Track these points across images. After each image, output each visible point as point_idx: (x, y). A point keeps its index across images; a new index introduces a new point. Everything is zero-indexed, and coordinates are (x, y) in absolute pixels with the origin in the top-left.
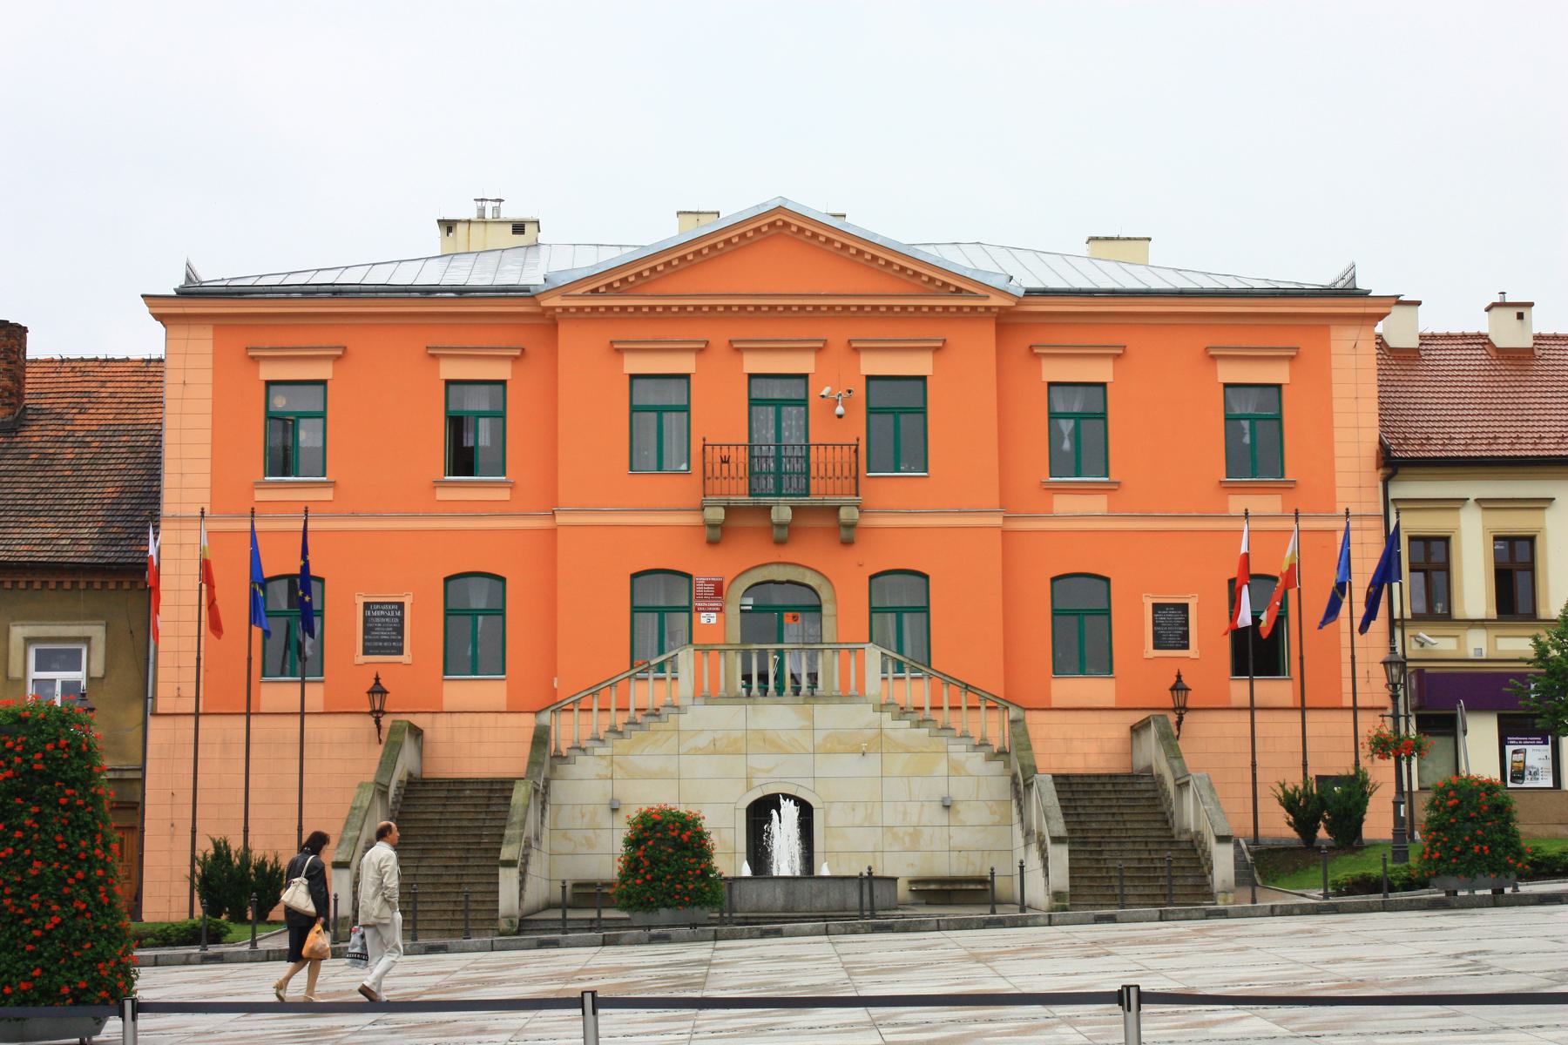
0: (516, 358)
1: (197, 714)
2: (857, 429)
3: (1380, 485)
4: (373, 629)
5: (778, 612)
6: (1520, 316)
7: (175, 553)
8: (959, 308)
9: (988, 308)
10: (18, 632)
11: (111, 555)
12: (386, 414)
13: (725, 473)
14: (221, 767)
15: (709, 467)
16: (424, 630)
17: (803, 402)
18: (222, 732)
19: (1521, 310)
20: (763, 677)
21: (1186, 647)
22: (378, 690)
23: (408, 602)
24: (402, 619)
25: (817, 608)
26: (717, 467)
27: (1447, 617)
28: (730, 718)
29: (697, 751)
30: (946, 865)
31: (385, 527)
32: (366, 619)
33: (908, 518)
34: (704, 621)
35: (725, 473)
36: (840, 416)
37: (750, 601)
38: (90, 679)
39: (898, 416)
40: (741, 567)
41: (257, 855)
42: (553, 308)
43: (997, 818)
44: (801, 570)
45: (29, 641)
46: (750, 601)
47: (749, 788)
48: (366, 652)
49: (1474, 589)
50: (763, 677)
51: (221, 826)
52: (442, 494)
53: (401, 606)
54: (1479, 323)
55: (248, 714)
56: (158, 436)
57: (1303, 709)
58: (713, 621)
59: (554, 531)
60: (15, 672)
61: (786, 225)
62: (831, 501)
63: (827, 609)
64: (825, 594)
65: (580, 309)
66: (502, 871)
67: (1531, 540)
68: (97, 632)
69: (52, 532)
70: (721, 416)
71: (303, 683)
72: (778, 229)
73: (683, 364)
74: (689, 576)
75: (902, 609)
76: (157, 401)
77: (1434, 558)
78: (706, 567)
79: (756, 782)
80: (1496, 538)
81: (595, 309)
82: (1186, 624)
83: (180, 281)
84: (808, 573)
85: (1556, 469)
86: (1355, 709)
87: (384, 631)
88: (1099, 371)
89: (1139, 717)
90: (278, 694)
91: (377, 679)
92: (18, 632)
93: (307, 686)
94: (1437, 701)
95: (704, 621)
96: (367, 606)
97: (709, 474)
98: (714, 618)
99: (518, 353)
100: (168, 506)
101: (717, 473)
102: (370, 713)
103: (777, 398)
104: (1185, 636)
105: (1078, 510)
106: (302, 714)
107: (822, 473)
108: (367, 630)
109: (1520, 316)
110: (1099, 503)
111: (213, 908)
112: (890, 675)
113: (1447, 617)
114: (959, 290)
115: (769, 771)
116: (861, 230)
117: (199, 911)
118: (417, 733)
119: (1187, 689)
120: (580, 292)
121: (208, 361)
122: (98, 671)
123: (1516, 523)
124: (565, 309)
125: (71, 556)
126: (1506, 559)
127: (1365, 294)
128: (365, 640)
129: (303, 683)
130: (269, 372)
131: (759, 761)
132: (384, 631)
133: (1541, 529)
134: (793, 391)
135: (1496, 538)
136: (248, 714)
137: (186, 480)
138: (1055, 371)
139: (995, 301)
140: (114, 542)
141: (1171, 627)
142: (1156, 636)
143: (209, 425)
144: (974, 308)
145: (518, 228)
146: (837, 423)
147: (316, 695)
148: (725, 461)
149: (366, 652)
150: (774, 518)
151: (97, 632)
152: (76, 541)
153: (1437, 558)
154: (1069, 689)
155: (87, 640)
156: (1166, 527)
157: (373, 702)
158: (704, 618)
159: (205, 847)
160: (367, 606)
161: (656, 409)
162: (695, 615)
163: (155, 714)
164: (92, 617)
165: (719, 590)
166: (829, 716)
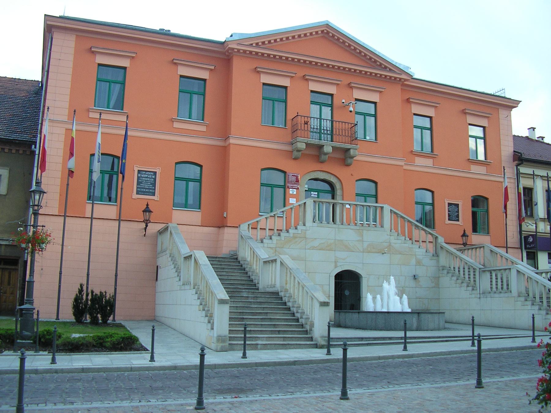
0: (211, 70)
3: (515, 167)
4: (141, 183)
8: (391, 77)
9: (400, 79)
13: (306, 129)
17: (331, 106)
21: (458, 220)
22: (147, 210)
23: (158, 171)
24: (155, 179)
26: (303, 125)
29: (313, 248)
31: (164, 135)
32: (138, 178)
34: (291, 192)
35: (306, 129)
36: (351, 111)
40: (305, 172)
42: (233, 49)
43: (433, 285)
44: (329, 175)
48: (137, 193)
52: (176, 125)
53: (155, 173)
57: (65, 216)
58: (295, 193)
61: (328, 33)
64: (338, 186)
65: (245, 51)
71: (93, 204)
72: (328, 34)
73: (285, 82)
74: (285, 172)
78: (290, 167)
79: (339, 264)
81: (251, 52)
82: (458, 212)
84: (332, 177)
85: (545, 166)
86: (92, 218)
91: (147, 205)
93: (95, 205)
95: (291, 192)
96: (139, 171)
98: (295, 192)
99: (213, 68)
101: (303, 128)
102: (143, 221)
104: (458, 216)
107: (338, 133)
108: (139, 183)
110: (429, 162)
114: (390, 70)
115: (344, 259)
116: (354, 37)
119: (468, 236)
120: (246, 44)
121: (72, 51)
124: (239, 50)
128: (137, 188)
129: (93, 204)
132: (147, 185)
137: (57, 106)
139: (403, 76)
142: (449, 215)
144: (395, 78)
149: (137, 193)
158: (292, 191)
160: (139, 171)
162: (287, 190)
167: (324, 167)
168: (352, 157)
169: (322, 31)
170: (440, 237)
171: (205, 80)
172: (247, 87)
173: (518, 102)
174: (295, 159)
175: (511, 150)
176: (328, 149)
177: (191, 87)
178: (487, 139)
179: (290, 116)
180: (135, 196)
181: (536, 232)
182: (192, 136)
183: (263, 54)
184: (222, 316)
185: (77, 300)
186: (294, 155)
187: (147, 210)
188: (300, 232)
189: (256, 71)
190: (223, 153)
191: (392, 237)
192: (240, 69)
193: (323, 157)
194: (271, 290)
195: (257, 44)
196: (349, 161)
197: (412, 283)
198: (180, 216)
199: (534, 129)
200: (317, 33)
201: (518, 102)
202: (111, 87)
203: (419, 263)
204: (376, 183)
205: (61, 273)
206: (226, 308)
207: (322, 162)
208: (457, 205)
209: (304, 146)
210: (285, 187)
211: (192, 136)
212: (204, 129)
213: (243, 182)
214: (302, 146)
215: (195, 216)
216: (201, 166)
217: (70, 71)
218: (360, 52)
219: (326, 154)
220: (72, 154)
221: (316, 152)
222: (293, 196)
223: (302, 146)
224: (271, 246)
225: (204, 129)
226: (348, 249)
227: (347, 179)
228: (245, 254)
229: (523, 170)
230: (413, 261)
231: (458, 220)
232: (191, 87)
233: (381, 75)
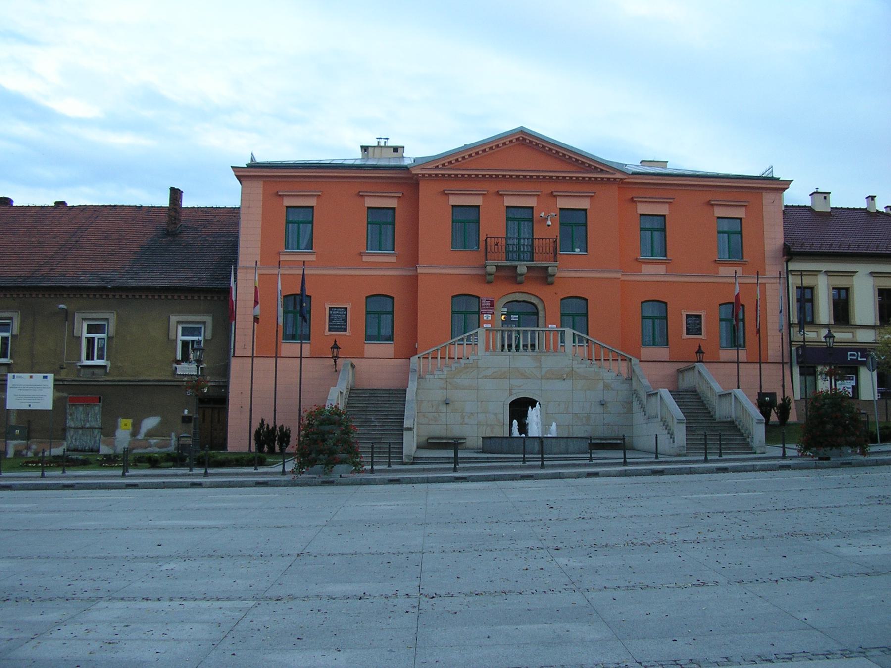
1: (253, 357)
2: (556, 232)
5: (529, 313)
6: (825, 198)
7: (244, 287)
9: (615, 179)
10: (174, 319)
11: (217, 285)
12: (341, 220)
14: (265, 384)
15: (489, 248)
16: (356, 320)
17: (531, 220)
18: (265, 365)
19: (826, 195)
20: (510, 346)
21: (701, 334)
22: (335, 347)
23: (349, 307)
24: (346, 315)
25: (537, 314)
27: (812, 323)
28: (503, 360)
29: (486, 377)
30: (601, 432)
32: (330, 315)
33: (574, 272)
37: (506, 310)
38: (206, 341)
39: (574, 224)
40: (503, 295)
41: (278, 425)
42: (417, 174)
45: (179, 322)
46: (506, 310)
47: (511, 395)
48: (329, 330)
49: (824, 312)
50: (510, 346)
51: (263, 413)
52: (365, 259)
53: (346, 309)
54: (808, 202)
55: (276, 357)
56: (237, 237)
59: (417, 276)
60: (172, 337)
61: (524, 139)
62: (545, 264)
63: (541, 314)
64: (540, 307)
65: (430, 175)
66: (405, 433)
67: (847, 290)
68: (208, 319)
69: (190, 275)
70: (493, 225)
71: (302, 344)
72: (523, 140)
74: (479, 298)
75: (576, 312)
76: (237, 224)
77: (807, 297)
79: (514, 392)
80: (833, 289)
81: (437, 175)
82: (701, 324)
83: (249, 162)
87: (338, 321)
88: (663, 210)
89: (682, 366)
90: (290, 348)
92: (174, 319)
94: (809, 360)
97: (489, 250)
100: (241, 262)
103: (521, 217)
104: (700, 329)
105: (653, 272)
106: (301, 357)
108: (330, 320)
109: (825, 198)
110: (661, 269)
111: (260, 448)
112: (577, 344)
113: (812, 323)
114: (602, 170)
117: (253, 449)
118: (353, 366)
122: (209, 337)
123: (842, 282)
124: (423, 175)
125: (198, 285)
126: (837, 298)
127: (778, 179)
129: (302, 344)
130: (288, 202)
131: (515, 382)
132: (338, 321)
133: (852, 285)
134: (525, 214)
135: (833, 289)
136: (276, 357)
137: (250, 248)
138: (643, 209)
140: (218, 279)
141: (694, 325)
142: (687, 329)
143: (260, 226)
144: (609, 179)
145: (396, 149)
146: (549, 224)
147: (307, 348)
148: (496, 245)
149: (329, 330)
150: (519, 270)
151: (208, 319)
152: (200, 279)
153: (808, 296)
154: (647, 352)
155: (204, 323)
156: (691, 279)
157: (333, 353)
158: (485, 317)
159: (256, 426)
161: (466, 220)
163: (234, 356)
164: (206, 312)
165: (492, 305)
166: (550, 362)
167: (523, 288)
168: (554, 275)
169: (518, 139)
170: (633, 359)
171: (394, 209)
172: (435, 214)
173: (788, 182)
174: (489, 282)
175: (780, 242)
176: (522, 269)
177: (380, 219)
178: (744, 233)
179: (482, 238)
180: (327, 333)
181: (804, 341)
182: (381, 269)
183: (450, 175)
184: (681, 436)
185: (258, 433)
186: (485, 279)
187: (335, 347)
188: (471, 361)
189: (444, 193)
190: (414, 280)
191: (575, 362)
192: (426, 191)
193: (519, 278)
194: (729, 419)
195: (443, 165)
196: (550, 279)
197: (599, 409)
198: (371, 349)
199: (873, 198)
200: (511, 141)
201: (788, 182)
202: (298, 226)
203: (607, 387)
204: (586, 300)
205: (251, 410)
206: (683, 427)
207: (520, 283)
208: (699, 317)
209: (494, 269)
210: (479, 313)
211: (381, 269)
212: (394, 259)
213: (434, 309)
214: (493, 269)
215: (387, 349)
216: (392, 298)
217: (260, 217)
218: (564, 155)
219: (521, 275)
220: (256, 303)
221: (510, 275)
222: (487, 322)
223: (493, 269)
224: (442, 376)
225: (394, 259)
226: (523, 376)
227: (549, 300)
228: (702, 388)
229: (792, 266)
230: (600, 386)
231: (701, 334)
232: (380, 219)
233: (590, 178)
